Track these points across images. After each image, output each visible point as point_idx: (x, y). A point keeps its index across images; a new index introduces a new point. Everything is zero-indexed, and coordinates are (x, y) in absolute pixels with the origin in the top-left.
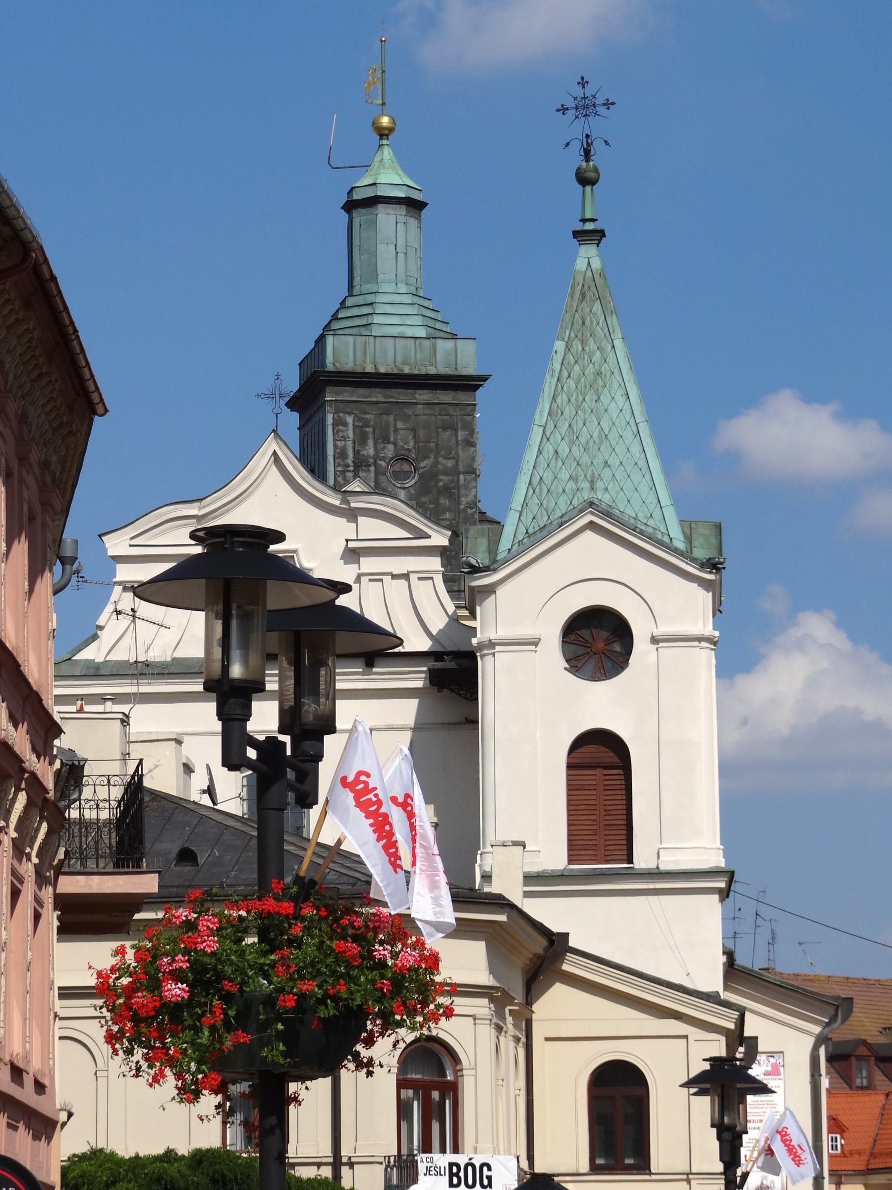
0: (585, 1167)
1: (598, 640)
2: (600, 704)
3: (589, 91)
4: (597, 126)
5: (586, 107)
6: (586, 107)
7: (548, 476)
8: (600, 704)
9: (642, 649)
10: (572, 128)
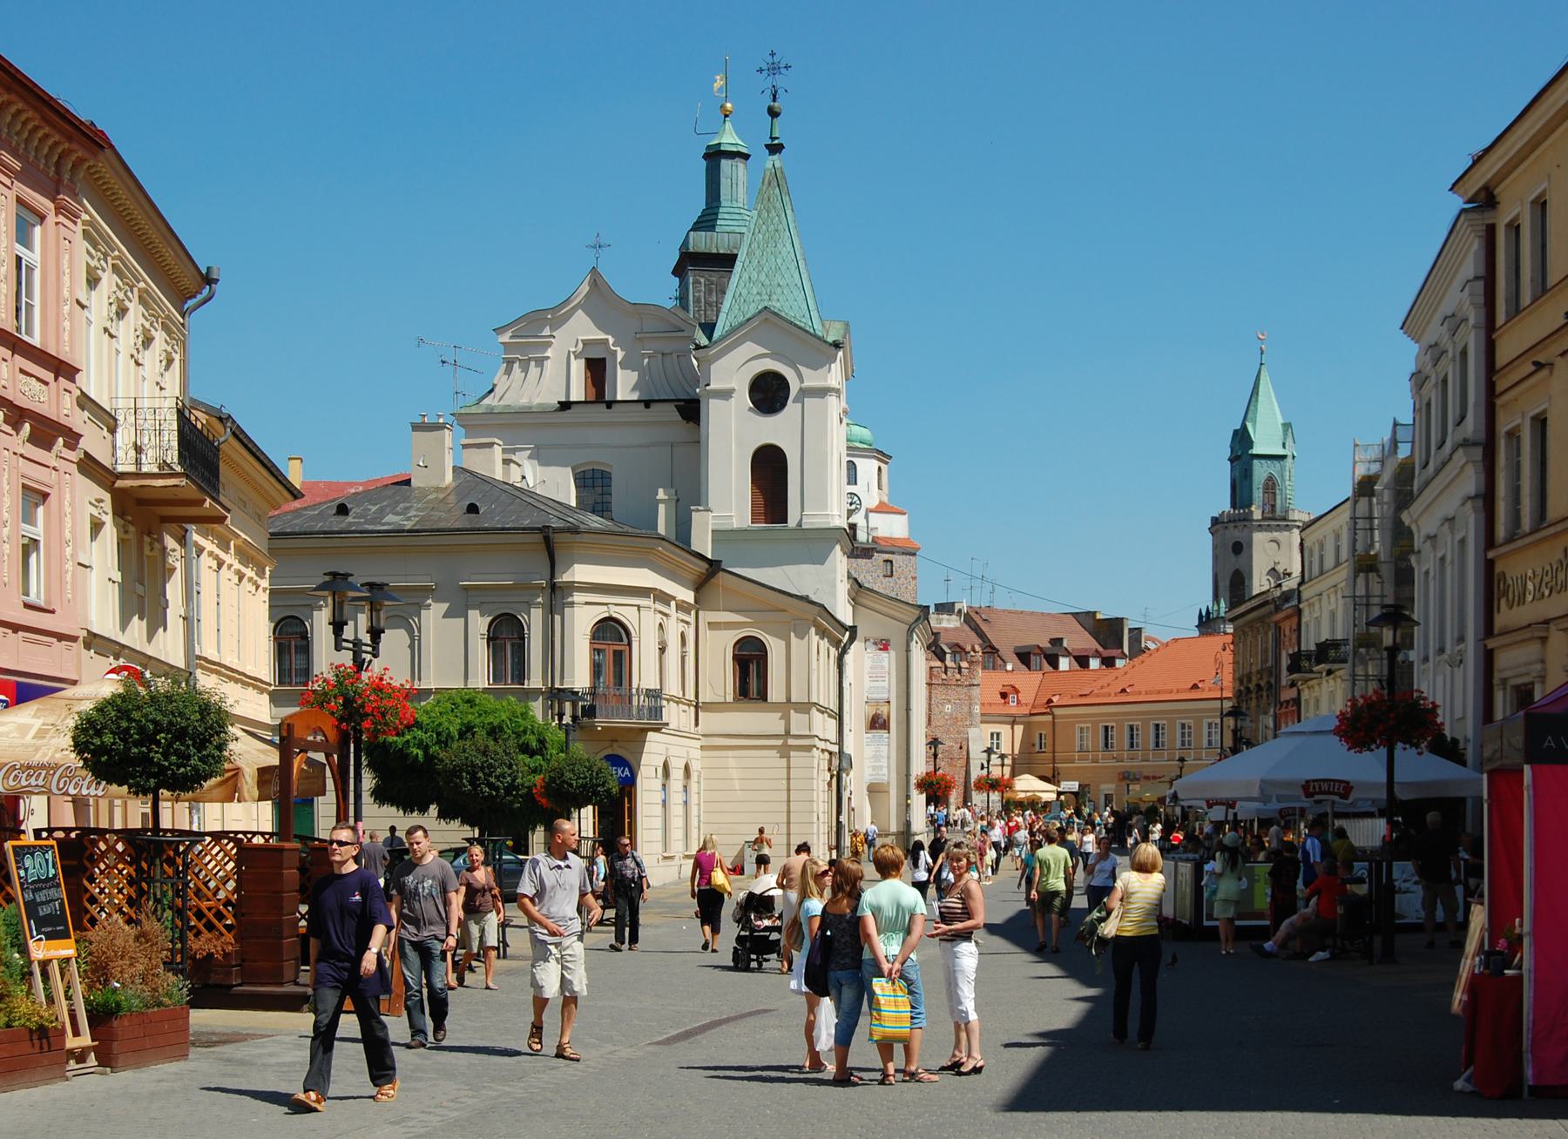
0: (730, 698)
1: (769, 394)
2: (776, 430)
3: (776, 59)
4: (780, 81)
6: (774, 69)
7: (744, 292)
8: (776, 430)
9: (792, 408)
10: (766, 82)
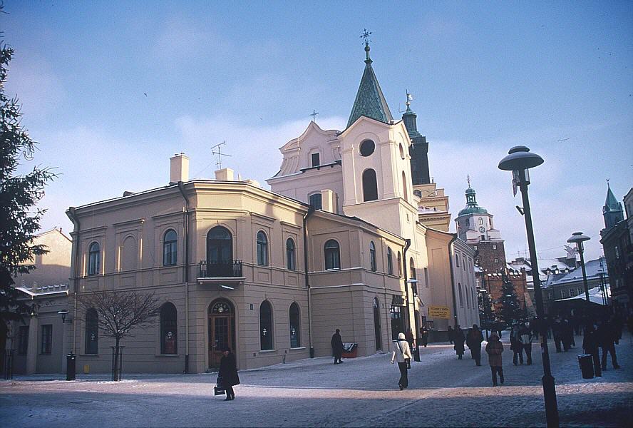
5: (366, 35)
6: (366, 35)
